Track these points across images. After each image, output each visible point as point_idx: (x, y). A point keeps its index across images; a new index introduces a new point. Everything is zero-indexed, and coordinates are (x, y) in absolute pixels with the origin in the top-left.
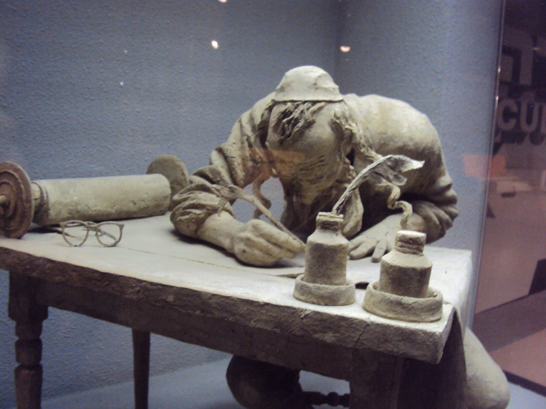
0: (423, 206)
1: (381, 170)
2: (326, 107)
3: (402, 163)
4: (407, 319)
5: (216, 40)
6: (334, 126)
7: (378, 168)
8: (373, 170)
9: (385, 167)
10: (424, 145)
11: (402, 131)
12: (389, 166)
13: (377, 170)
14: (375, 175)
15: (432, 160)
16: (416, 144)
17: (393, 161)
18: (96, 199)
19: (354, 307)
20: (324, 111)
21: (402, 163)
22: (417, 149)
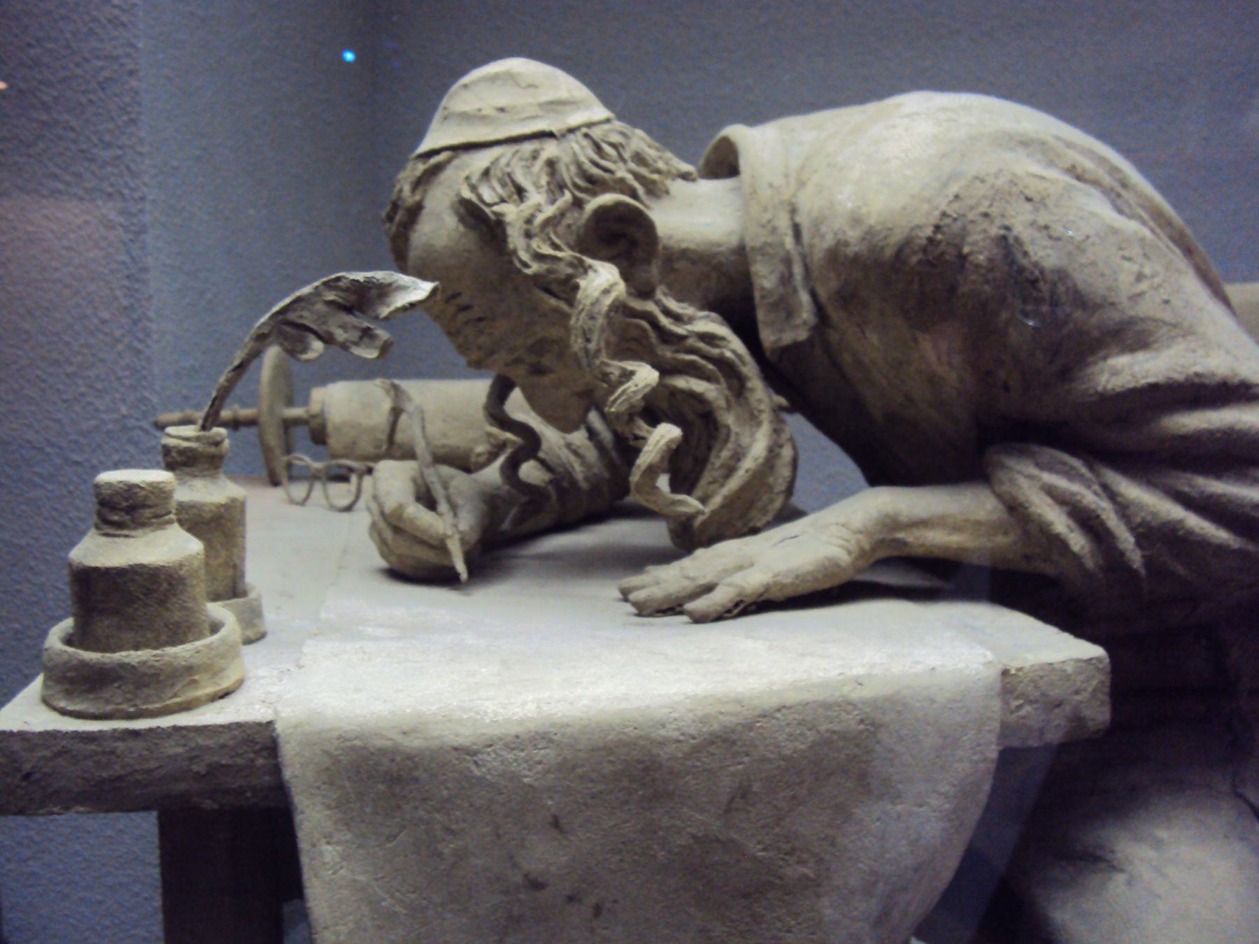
0: (1011, 462)
1: (308, 319)
2: (456, 162)
3: (384, 291)
4: (71, 708)
5: (349, 50)
6: (462, 210)
7: (295, 310)
8: (280, 317)
9: (320, 307)
10: (897, 237)
11: (840, 197)
12: (330, 303)
13: (292, 316)
14: (288, 329)
15: (963, 289)
16: (870, 233)
17: (346, 290)
18: (444, 421)
19: (610, 737)
20: (448, 173)
21: (384, 291)
22: (875, 250)
